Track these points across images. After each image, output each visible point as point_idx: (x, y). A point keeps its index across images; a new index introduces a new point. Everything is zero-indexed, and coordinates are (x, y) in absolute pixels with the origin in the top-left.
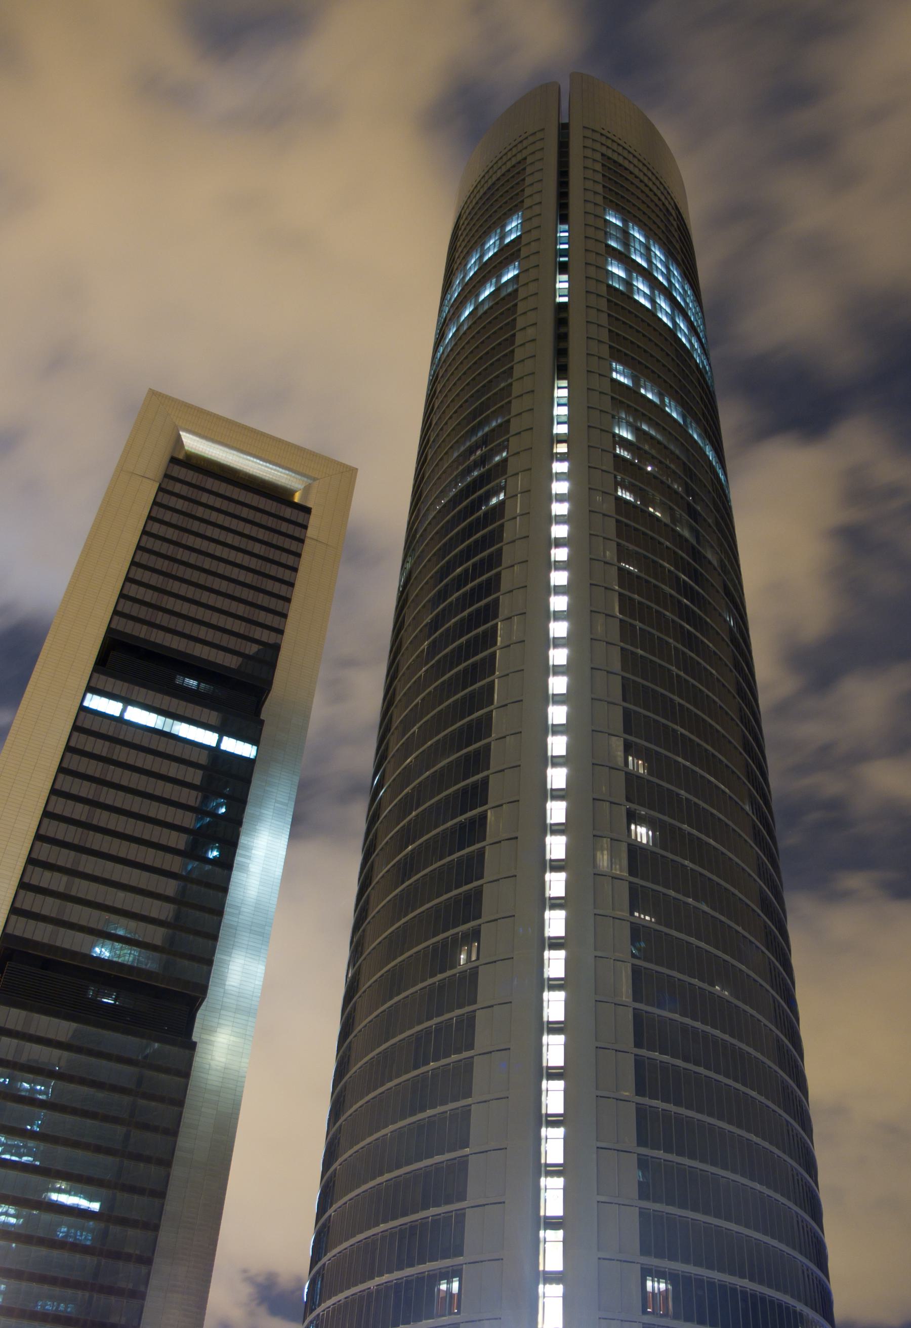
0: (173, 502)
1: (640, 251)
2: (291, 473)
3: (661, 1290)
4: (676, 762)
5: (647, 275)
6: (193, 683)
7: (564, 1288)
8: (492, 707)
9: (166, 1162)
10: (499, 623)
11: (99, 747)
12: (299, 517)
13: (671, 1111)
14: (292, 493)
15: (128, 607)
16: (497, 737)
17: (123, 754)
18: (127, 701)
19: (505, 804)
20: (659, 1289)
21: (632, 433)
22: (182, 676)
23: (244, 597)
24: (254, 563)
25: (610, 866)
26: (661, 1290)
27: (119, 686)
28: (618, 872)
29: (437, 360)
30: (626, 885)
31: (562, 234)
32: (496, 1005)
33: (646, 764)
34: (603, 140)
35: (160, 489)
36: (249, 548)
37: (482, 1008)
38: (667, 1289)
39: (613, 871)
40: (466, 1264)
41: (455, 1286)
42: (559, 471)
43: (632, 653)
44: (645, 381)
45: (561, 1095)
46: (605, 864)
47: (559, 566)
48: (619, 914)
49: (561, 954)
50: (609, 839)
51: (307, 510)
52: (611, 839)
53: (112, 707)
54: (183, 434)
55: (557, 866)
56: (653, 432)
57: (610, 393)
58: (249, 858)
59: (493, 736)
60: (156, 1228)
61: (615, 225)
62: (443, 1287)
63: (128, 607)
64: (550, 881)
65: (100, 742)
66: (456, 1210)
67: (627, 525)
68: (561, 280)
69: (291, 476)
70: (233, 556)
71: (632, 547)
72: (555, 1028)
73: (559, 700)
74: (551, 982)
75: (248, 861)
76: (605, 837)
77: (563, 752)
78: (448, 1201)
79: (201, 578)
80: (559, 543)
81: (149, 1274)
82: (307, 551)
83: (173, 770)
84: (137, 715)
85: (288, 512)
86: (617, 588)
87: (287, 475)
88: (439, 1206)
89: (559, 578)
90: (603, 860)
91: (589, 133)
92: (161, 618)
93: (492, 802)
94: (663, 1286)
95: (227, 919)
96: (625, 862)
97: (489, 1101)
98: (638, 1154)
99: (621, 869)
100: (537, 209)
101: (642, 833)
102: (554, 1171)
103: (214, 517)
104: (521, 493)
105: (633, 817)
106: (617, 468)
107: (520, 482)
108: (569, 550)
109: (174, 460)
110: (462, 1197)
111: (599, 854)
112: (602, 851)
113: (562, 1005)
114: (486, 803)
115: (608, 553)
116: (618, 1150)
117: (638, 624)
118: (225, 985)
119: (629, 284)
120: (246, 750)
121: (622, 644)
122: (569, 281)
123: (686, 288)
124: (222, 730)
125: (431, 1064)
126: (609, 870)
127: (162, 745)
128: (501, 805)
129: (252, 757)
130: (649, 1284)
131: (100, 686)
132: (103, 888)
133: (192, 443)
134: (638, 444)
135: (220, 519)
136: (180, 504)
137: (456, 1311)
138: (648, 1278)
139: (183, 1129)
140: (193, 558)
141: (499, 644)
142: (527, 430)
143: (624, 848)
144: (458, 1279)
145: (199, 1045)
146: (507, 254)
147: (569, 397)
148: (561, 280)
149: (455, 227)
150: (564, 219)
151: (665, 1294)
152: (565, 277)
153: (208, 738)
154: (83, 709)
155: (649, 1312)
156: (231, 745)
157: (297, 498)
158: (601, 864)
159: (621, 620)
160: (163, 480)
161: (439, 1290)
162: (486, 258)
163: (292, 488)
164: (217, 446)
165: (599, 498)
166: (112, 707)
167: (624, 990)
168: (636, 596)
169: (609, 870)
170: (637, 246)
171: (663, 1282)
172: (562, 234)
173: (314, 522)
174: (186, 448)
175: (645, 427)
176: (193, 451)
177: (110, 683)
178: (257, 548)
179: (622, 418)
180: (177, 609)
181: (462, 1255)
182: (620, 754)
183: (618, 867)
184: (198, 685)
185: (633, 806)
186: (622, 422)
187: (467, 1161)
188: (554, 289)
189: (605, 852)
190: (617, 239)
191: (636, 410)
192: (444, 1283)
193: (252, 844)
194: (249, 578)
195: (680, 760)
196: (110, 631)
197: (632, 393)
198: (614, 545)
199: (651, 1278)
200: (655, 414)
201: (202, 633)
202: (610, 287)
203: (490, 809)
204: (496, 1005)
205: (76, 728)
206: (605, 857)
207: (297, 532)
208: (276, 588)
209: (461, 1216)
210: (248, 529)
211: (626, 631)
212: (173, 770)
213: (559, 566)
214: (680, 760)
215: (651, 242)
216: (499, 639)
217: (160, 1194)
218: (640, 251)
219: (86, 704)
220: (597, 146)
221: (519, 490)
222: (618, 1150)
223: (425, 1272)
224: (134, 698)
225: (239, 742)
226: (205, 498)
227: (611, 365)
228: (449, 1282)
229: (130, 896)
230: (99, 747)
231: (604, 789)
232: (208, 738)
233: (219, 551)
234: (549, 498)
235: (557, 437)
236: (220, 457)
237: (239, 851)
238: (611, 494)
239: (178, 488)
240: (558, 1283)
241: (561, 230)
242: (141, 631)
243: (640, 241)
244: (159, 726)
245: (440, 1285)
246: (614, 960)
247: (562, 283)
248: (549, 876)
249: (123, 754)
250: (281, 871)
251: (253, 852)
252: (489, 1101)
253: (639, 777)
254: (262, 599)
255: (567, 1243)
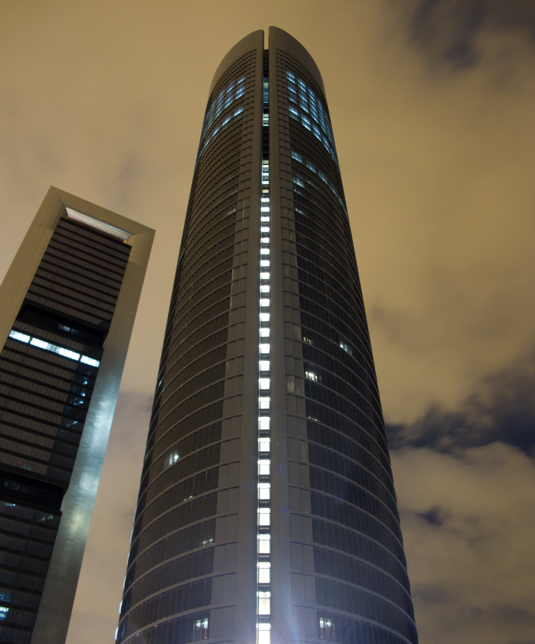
0: (61, 239)
1: (305, 105)
2: (121, 231)
3: (328, 626)
4: (329, 341)
5: (309, 116)
6: (67, 329)
7: (267, 184)
8: (229, 310)
9: (43, 576)
10: (233, 270)
11: (17, 358)
12: (125, 250)
13: (332, 524)
14: (123, 240)
15: (36, 289)
16: (231, 325)
17: (29, 362)
18: (32, 336)
19: (236, 358)
20: (327, 625)
21: (303, 184)
22: (62, 325)
23: (96, 287)
24: (101, 271)
25: (295, 390)
26: (328, 626)
27: (30, 328)
28: (299, 394)
29: (199, 158)
30: (304, 400)
31: (265, 119)
32: (230, 463)
33: (313, 343)
34: (286, 56)
35: (55, 233)
36: (99, 264)
37: (222, 465)
38: (332, 626)
39: (297, 393)
40: (212, 609)
41: (206, 623)
42: (264, 221)
43: (305, 286)
44: (308, 162)
45: (268, 543)
46: (292, 389)
47: (264, 296)
48: (300, 415)
49: (267, 485)
50: (294, 377)
51: (130, 247)
52: (296, 377)
53: (24, 338)
54: (68, 209)
55: (264, 479)
56: (313, 186)
57: (293, 199)
58: (94, 419)
59: (229, 324)
60: (36, 611)
61: (292, 82)
62: (199, 624)
63: (36, 289)
64: (260, 465)
65: (17, 355)
66: (207, 578)
67: (301, 226)
68: (264, 163)
69: (121, 232)
70: (91, 267)
71: (303, 236)
72: (264, 479)
73: (265, 357)
74: (261, 502)
75: (93, 421)
76: (292, 375)
77: (267, 407)
78: (202, 574)
79: (75, 277)
80: (264, 282)
81: (31, 636)
82: (129, 267)
83: (55, 371)
84: (37, 343)
85: (120, 248)
86: (296, 254)
87: (120, 231)
88: (196, 576)
89: (265, 303)
90: (291, 387)
91: (279, 52)
92: (52, 295)
93: (228, 357)
94: (329, 624)
95: (80, 450)
96: (303, 389)
97: (226, 516)
98: (314, 547)
99: (301, 392)
100: (251, 105)
101: (311, 375)
102: (264, 558)
103: (82, 247)
104: (245, 208)
105: (307, 368)
106: (295, 198)
107: (244, 204)
108: (270, 346)
109: (62, 219)
110: (211, 570)
111: (289, 384)
112: (290, 382)
113: (268, 516)
114: (225, 358)
115: (291, 237)
116: (302, 544)
117: (308, 272)
118: (79, 484)
119: (300, 119)
120: (94, 363)
121: (300, 281)
122: (269, 118)
123: (331, 151)
124: (82, 353)
125: (192, 578)
126: (294, 392)
127: (50, 359)
128: (234, 359)
129: (97, 366)
130: (322, 622)
131: (18, 327)
132: (15, 430)
133: (72, 213)
134: (305, 189)
135: (85, 249)
136: (64, 240)
137: (206, 638)
138: (321, 618)
139: (53, 558)
140: (70, 267)
141: (232, 279)
142: (248, 163)
143: (302, 382)
144: (207, 619)
145: (63, 514)
146: (236, 105)
147: (269, 168)
148: (264, 163)
149: (211, 96)
150: (265, 131)
151: (331, 629)
152: (267, 162)
153: (74, 356)
154: (10, 339)
155: (321, 638)
156: (86, 360)
157: (125, 242)
158: (290, 389)
159: (299, 270)
160: (56, 228)
161: (196, 627)
162: (226, 107)
163: (122, 238)
164: (84, 216)
165: (286, 211)
166: (24, 338)
167: (304, 456)
168: (306, 259)
169: (294, 392)
170: (303, 103)
171: (329, 621)
172: (265, 119)
173: (132, 253)
174: (69, 216)
175: (309, 182)
176: (72, 218)
177: (24, 326)
178: (103, 264)
179: (298, 177)
180: (61, 291)
181: (210, 604)
182: (299, 334)
183: (299, 391)
184: (71, 330)
185: (308, 361)
186: (297, 178)
187: (212, 581)
188: (262, 121)
189: (292, 383)
190: (293, 98)
191: (304, 174)
192: (199, 622)
193: (96, 412)
194: (99, 278)
195: (331, 340)
196: (26, 300)
197: (303, 166)
198: (294, 234)
199: (322, 619)
200: (314, 178)
201: (74, 304)
202: (290, 118)
203: (227, 361)
204: (230, 463)
205: (5, 348)
206: (292, 386)
207: (124, 257)
208: (113, 284)
209: (210, 581)
210: (99, 254)
211: (301, 274)
212: (55, 371)
213: (264, 296)
214: (331, 340)
215: (313, 126)
216: (233, 277)
217: (39, 593)
218: (305, 105)
219: (11, 336)
220: (284, 62)
221: (244, 207)
222: (302, 544)
223: (188, 615)
224: (36, 334)
225: (90, 359)
226: (77, 238)
227: (291, 152)
228: (202, 621)
229: (30, 434)
230: (17, 358)
231: (291, 351)
232: (74, 356)
233: (83, 264)
234: (260, 214)
235: (263, 186)
236: (86, 221)
237: (88, 415)
238: (292, 210)
239: (64, 232)
240: (266, 622)
241: (265, 95)
242: (42, 301)
243: (305, 101)
244: (49, 349)
245: (196, 623)
246: (298, 440)
247: (266, 118)
248: (261, 440)
249: (29, 362)
250: (111, 426)
251: (96, 416)
252: (226, 516)
253: (310, 347)
254: (104, 289)
255: (272, 570)
